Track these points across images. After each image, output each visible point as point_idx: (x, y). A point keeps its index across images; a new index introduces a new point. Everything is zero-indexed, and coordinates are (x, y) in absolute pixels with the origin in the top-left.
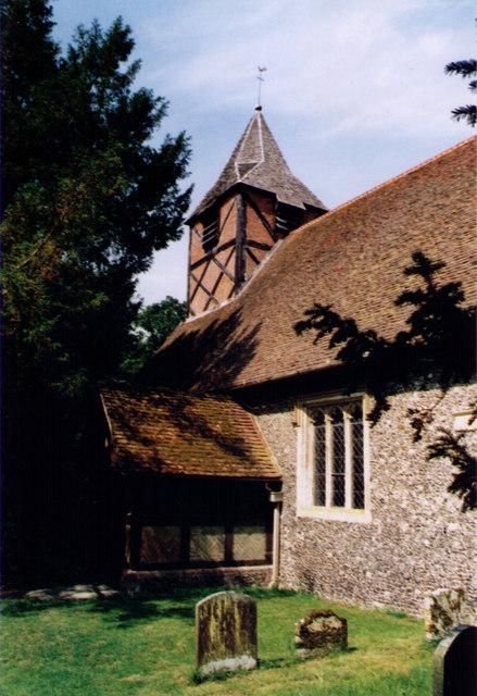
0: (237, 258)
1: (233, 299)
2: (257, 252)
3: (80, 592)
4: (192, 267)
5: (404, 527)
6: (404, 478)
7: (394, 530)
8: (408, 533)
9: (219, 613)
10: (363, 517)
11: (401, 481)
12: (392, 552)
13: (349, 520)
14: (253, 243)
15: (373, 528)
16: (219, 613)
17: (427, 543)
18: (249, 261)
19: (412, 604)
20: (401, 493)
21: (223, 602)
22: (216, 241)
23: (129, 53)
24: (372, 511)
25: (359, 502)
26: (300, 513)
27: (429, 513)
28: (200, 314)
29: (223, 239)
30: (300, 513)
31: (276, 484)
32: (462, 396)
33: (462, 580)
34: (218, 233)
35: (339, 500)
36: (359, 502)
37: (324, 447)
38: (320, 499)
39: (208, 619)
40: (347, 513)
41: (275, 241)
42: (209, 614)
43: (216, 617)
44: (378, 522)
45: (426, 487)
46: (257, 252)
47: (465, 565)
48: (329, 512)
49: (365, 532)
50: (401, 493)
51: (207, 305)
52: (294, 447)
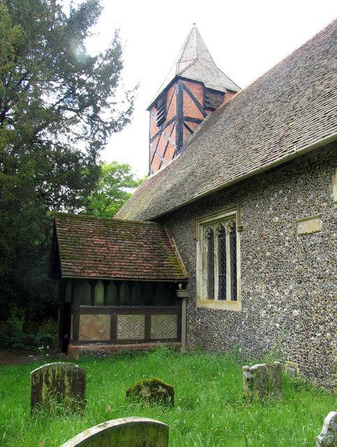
0: (177, 130)
1: (175, 159)
2: (190, 125)
4: (151, 141)
5: (263, 313)
6: (263, 275)
7: (256, 316)
9: (50, 379)
11: (261, 278)
12: (255, 333)
13: (228, 309)
14: (189, 119)
16: (50, 379)
17: (278, 325)
18: (185, 130)
19: (18, 381)
21: (54, 372)
22: (164, 120)
24: (242, 302)
25: (234, 298)
26: (199, 305)
27: (280, 302)
28: (62, 139)
29: (169, 117)
30: (199, 305)
31: (185, 283)
32: (303, 206)
33: (302, 355)
34: (165, 113)
35: (223, 296)
36: (234, 298)
38: (211, 296)
39: (40, 385)
42: (41, 380)
43: (47, 383)
45: (278, 282)
46: (190, 125)
47: (304, 343)
49: (237, 317)
51: (160, 166)
52: (195, 257)
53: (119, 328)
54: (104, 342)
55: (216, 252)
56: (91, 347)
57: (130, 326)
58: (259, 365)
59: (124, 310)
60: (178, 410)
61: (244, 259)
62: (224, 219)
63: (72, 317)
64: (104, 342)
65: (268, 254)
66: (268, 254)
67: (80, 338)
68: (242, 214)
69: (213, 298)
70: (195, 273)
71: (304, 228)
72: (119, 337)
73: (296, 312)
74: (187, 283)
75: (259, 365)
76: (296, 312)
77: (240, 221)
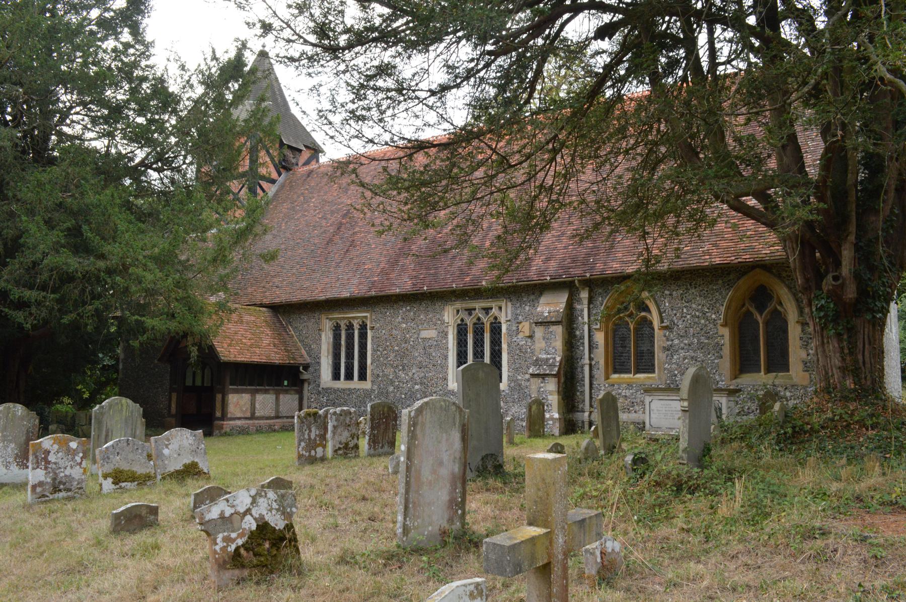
2: (264, 184)
3: (402, 25)
5: (391, 389)
8: (393, 392)
10: (367, 385)
15: (372, 390)
20: (389, 371)
23: (145, 415)
35: (349, 376)
36: (363, 377)
37: (340, 344)
38: (336, 377)
40: (355, 384)
41: (280, 174)
44: (375, 387)
45: (403, 367)
46: (264, 184)
48: (342, 384)
50: (389, 371)
53: (257, 406)
54: (246, 418)
55: (343, 343)
56: (238, 423)
57: (265, 402)
58: (426, 400)
59: (261, 390)
60: (776, 193)
61: (374, 350)
62: (354, 318)
63: (173, 406)
64: (246, 418)
65: (396, 348)
66: (396, 348)
67: (229, 416)
68: (374, 317)
69: (339, 379)
70: (319, 358)
71: (425, 334)
72: (257, 414)
73: (417, 387)
74: (311, 366)
75: (426, 400)
76: (417, 387)
77: (371, 322)
